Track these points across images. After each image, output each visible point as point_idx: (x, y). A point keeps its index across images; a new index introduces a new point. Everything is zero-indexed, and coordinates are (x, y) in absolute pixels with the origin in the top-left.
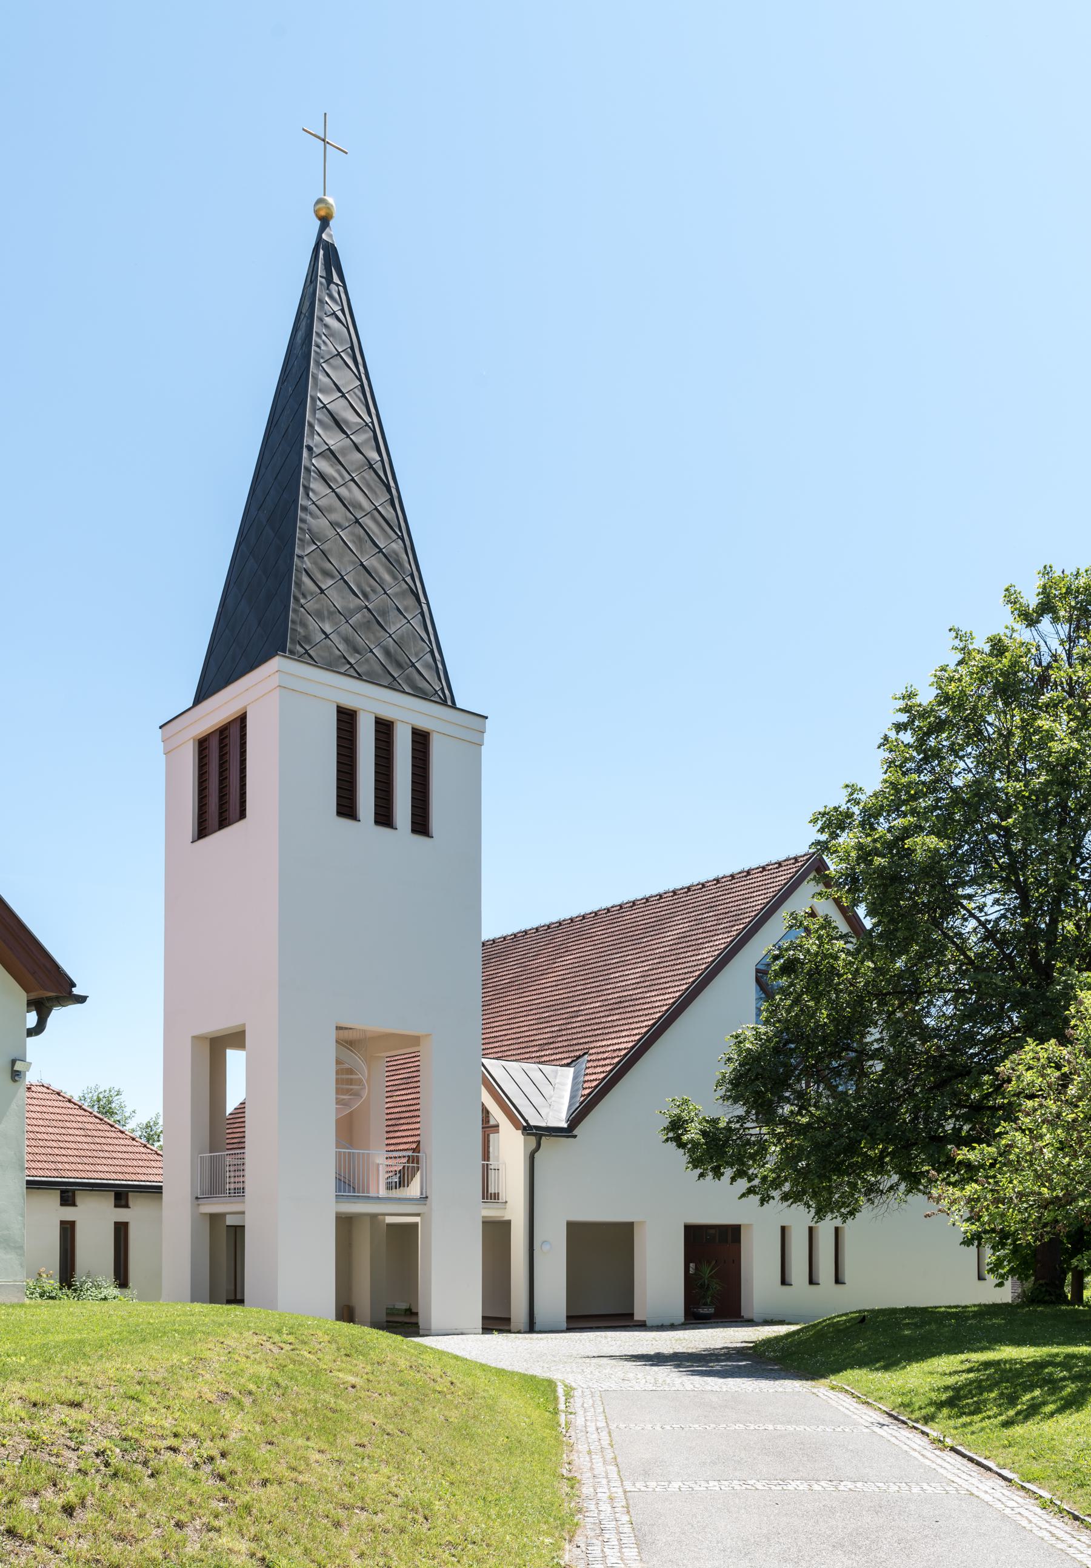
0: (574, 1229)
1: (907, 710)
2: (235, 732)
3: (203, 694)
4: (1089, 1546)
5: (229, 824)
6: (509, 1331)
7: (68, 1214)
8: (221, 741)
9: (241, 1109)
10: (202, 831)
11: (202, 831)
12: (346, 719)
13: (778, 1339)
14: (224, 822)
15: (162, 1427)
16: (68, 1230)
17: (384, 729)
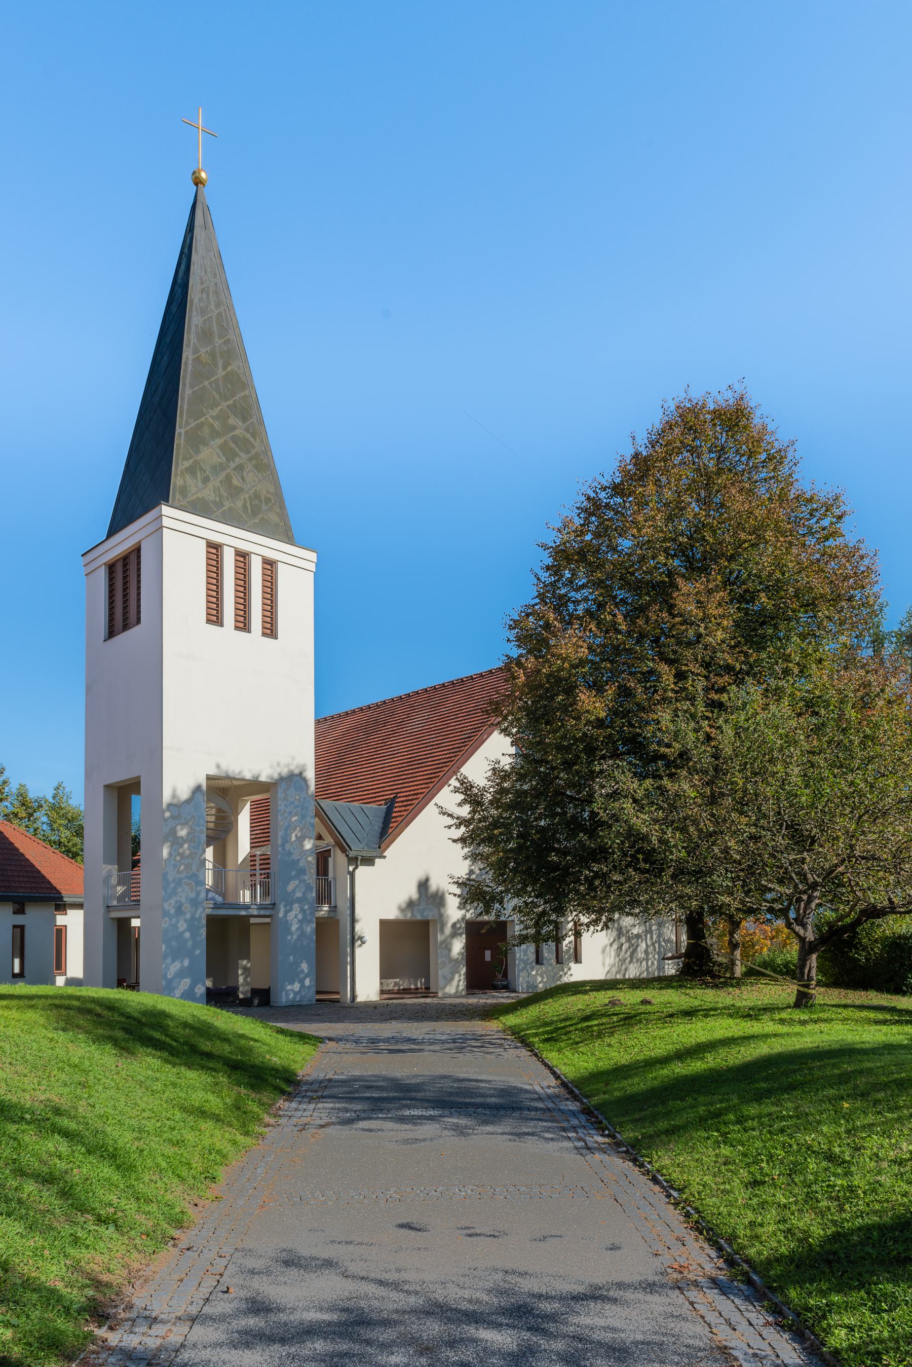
1: (494, 769)
2: (133, 558)
3: (112, 531)
4: (911, 1327)
5: (130, 628)
6: (381, 978)
8: (125, 565)
9: (208, 845)
10: (111, 633)
11: (111, 633)
12: (214, 549)
14: (126, 627)
17: (243, 557)
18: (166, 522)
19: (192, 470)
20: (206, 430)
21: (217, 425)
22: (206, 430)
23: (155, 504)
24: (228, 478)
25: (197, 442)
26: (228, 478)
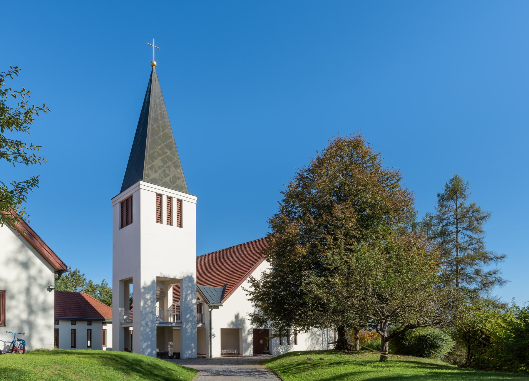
0: (222, 330)
2: (130, 200)
7: (74, 327)
10: (122, 226)
11: (122, 226)
12: (159, 196)
13: (192, 364)
14: (127, 224)
15: (485, 326)
16: (74, 331)
17: (170, 198)
18: (141, 187)
19: (151, 168)
20: (156, 154)
21: (160, 152)
22: (156, 154)
23: (138, 181)
24: (164, 171)
25: (153, 158)
26: (164, 171)
